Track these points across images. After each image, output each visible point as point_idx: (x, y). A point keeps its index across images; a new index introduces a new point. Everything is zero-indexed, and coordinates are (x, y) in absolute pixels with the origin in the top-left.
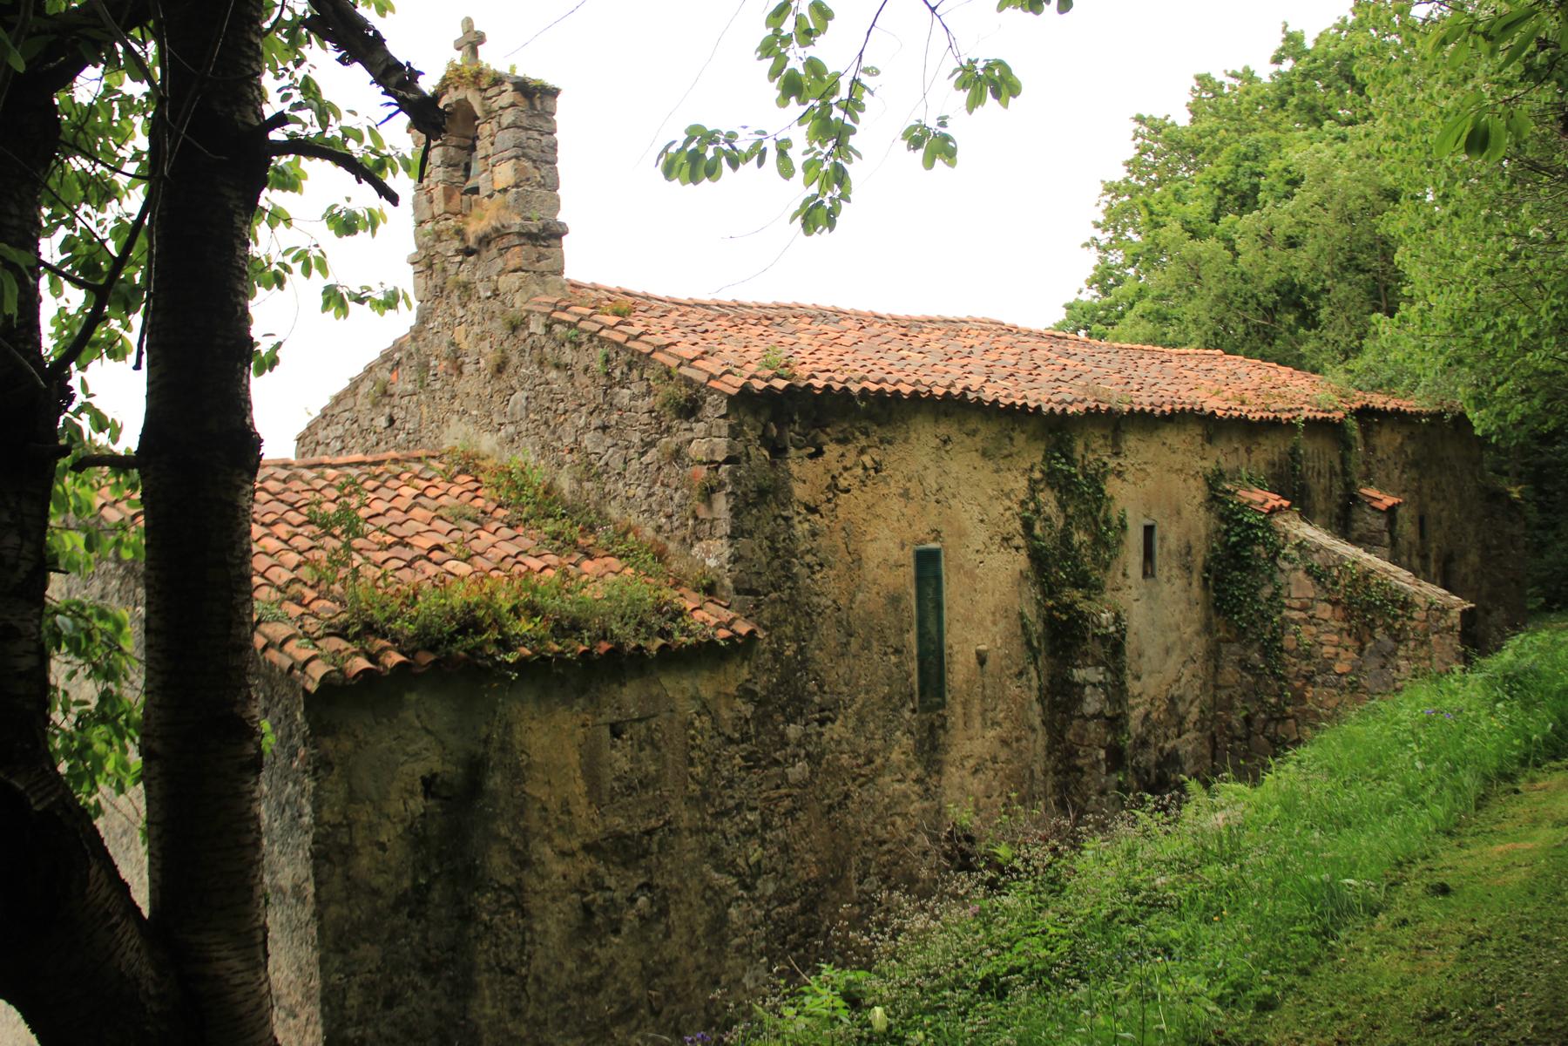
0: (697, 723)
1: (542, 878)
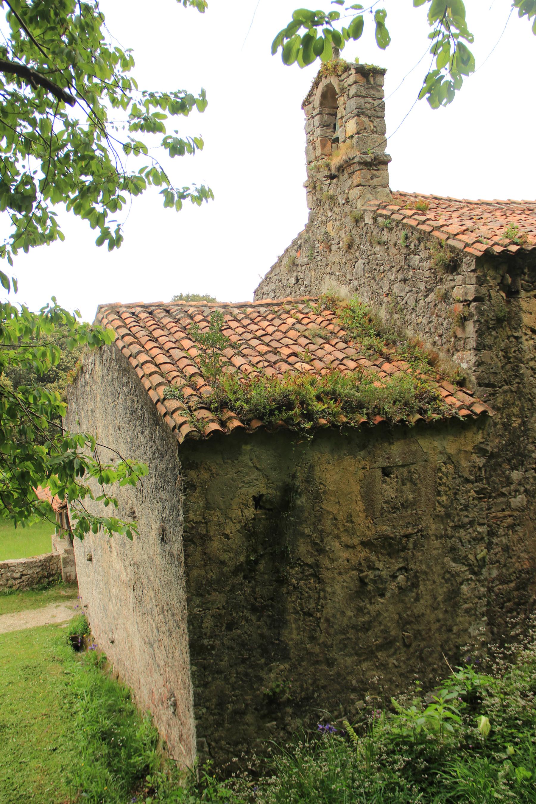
0: (444, 469)
1: (332, 560)
